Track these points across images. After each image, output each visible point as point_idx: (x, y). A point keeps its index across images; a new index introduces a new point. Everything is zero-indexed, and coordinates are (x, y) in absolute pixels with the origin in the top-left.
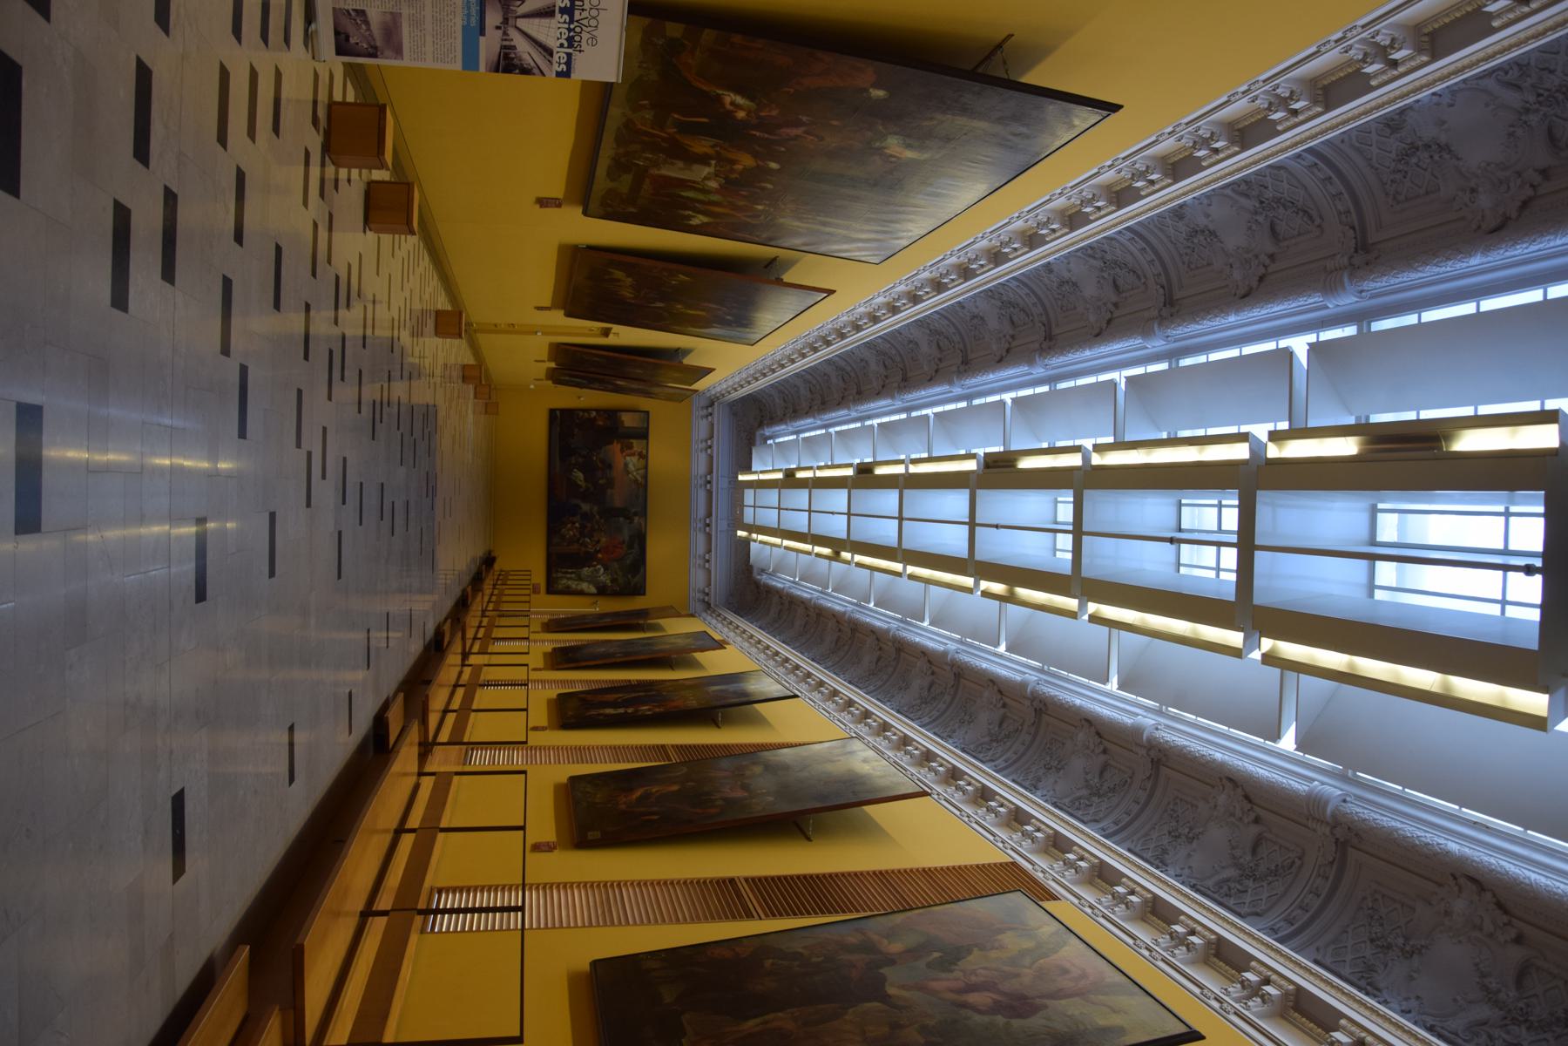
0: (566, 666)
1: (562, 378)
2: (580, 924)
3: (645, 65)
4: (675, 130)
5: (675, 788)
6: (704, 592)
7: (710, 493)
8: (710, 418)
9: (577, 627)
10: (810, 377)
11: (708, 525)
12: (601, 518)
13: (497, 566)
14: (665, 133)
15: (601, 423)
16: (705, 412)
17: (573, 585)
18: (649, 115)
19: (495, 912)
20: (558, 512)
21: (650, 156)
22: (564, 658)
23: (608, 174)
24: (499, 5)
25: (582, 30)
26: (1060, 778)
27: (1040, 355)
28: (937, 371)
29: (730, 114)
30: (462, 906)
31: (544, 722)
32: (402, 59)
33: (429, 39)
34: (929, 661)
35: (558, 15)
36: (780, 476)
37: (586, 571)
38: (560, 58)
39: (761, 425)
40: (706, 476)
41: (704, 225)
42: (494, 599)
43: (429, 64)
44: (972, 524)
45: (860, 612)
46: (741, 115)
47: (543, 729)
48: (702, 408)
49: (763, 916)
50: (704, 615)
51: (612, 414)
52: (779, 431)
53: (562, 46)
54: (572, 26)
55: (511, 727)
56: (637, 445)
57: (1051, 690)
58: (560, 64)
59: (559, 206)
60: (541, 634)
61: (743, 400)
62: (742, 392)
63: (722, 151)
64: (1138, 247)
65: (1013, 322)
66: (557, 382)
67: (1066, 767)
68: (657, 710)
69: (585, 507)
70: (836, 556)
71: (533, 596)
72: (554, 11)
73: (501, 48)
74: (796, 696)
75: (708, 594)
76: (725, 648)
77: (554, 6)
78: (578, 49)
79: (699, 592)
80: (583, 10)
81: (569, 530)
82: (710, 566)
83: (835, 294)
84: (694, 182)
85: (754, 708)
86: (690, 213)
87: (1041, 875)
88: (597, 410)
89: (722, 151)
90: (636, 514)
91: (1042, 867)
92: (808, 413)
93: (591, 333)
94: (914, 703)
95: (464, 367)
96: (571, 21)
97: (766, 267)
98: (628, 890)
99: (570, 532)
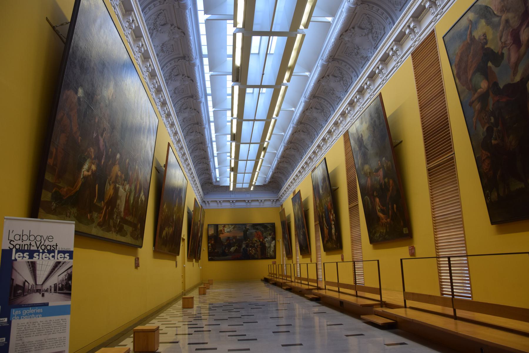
0: (309, 250)
1: (198, 256)
2: (462, 232)
3: (68, 214)
4: (102, 202)
5: (377, 200)
6: (272, 202)
7: (237, 201)
8: (209, 202)
9: (290, 247)
10: (195, 163)
11: (248, 201)
12: (247, 240)
13: (268, 277)
14: (104, 207)
15: (213, 242)
16: (207, 204)
17: (272, 249)
18: (95, 215)
19: (451, 269)
20: (246, 256)
21: (115, 215)
22: (305, 250)
23: (124, 236)
24: (28, 296)
25: (43, 245)
26: (362, 48)
27: (192, 61)
28: (195, 110)
29: (94, 173)
30: (450, 284)
31: (309, 259)
32: (65, 351)
33: (52, 336)
34: (307, 110)
35: (34, 260)
36: (232, 173)
37: (267, 245)
38: (61, 258)
39: (211, 183)
40: (231, 203)
41: (144, 194)
42: (273, 276)
43: (67, 335)
44: (261, 86)
45: (284, 140)
46: (94, 167)
47: (293, 261)
48: (206, 205)
49: (453, 153)
50: (281, 201)
51: (209, 238)
52: (214, 176)
53: (53, 257)
54: (41, 251)
55: (312, 267)
56: (220, 228)
57: (326, 53)
58: (65, 257)
59: (138, 258)
60: (293, 260)
61: (203, 190)
62: (201, 190)
63: (112, 180)
64: (148, 11)
65: (177, 75)
66: (199, 258)
67: (358, 46)
68: (333, 212)
69: (244, 246)
70: (265, 149)
71: (277, 264)
72: (32, 262)
73: (56, 292)
74: (325, 159)
75: (273, 200)
76: (299, 192)
77: (28, 262)
78: (55, 247)
79: (273, 204)
80: (30, 245)
81: (252, 252)
82: (263, 200)
83: (169, 142)
84: (126, 196)
85: (330, 173)
86: (140, 199)
87: (417, 43)
88: (208, 243)
89: (112, 180)
90: (246, 228)
91: (411, 44)
92: (208, 164)
93: (184, 246)
94: (323, 115)
95: (200, 294)
96: (38, 251)
97: (159, 173)
98: (436, 214)
99: (253, 252)
